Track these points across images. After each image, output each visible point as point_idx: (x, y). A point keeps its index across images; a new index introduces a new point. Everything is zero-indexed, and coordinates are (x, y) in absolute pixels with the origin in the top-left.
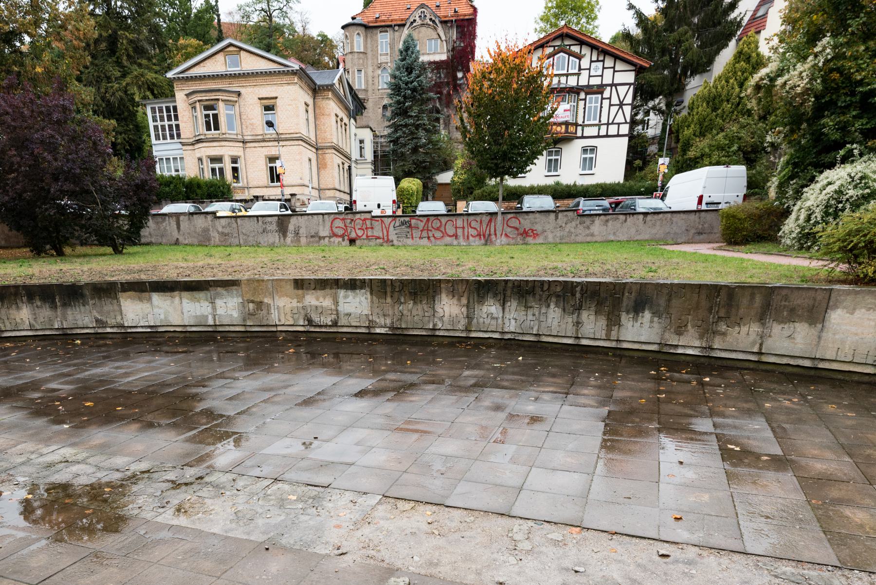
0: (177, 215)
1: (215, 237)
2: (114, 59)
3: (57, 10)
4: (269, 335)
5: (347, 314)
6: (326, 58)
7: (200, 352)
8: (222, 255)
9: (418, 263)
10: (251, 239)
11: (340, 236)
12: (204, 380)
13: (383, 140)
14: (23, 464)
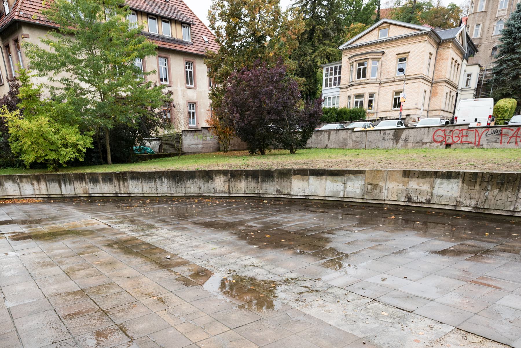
0: (329, 131)
1: (350, 143)
2: (311, 43)
3: (286, 20)
4: (378, 206)
5: (439, 196)
6: (452, 21)
7: (332, 213)
8: (353, 155)
9: (504, 161)
10: (373, 144)
11: (439, 142)
12: (333, 230)
13: (487, 72)
14: (233, 263)
